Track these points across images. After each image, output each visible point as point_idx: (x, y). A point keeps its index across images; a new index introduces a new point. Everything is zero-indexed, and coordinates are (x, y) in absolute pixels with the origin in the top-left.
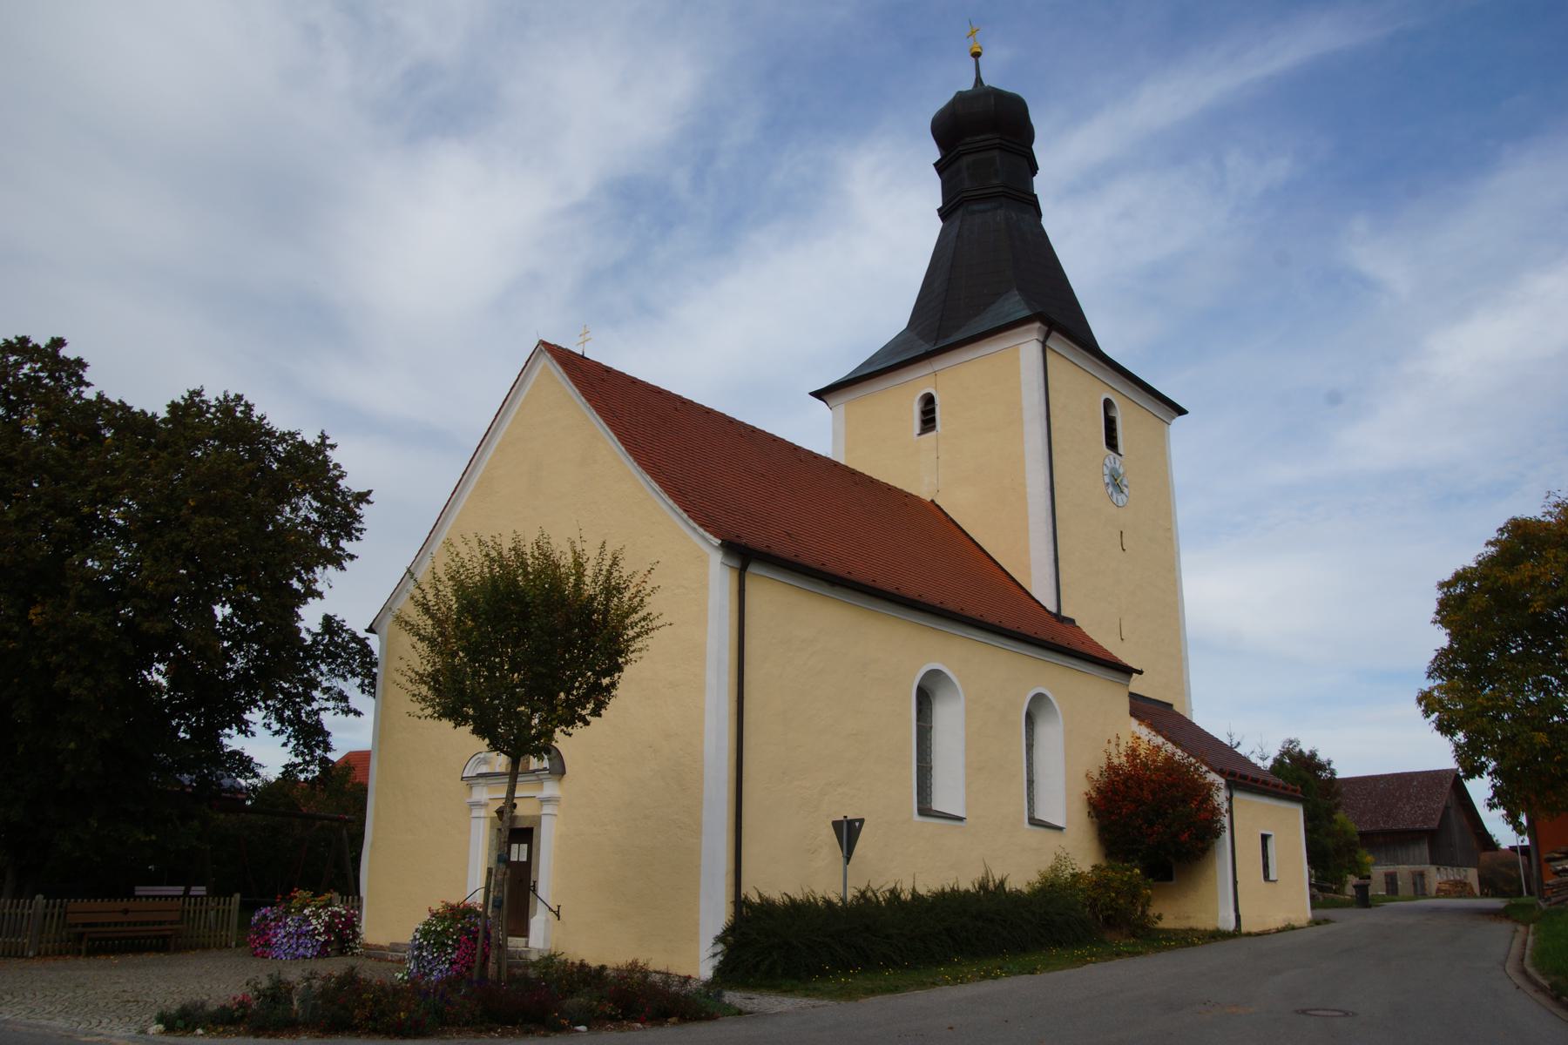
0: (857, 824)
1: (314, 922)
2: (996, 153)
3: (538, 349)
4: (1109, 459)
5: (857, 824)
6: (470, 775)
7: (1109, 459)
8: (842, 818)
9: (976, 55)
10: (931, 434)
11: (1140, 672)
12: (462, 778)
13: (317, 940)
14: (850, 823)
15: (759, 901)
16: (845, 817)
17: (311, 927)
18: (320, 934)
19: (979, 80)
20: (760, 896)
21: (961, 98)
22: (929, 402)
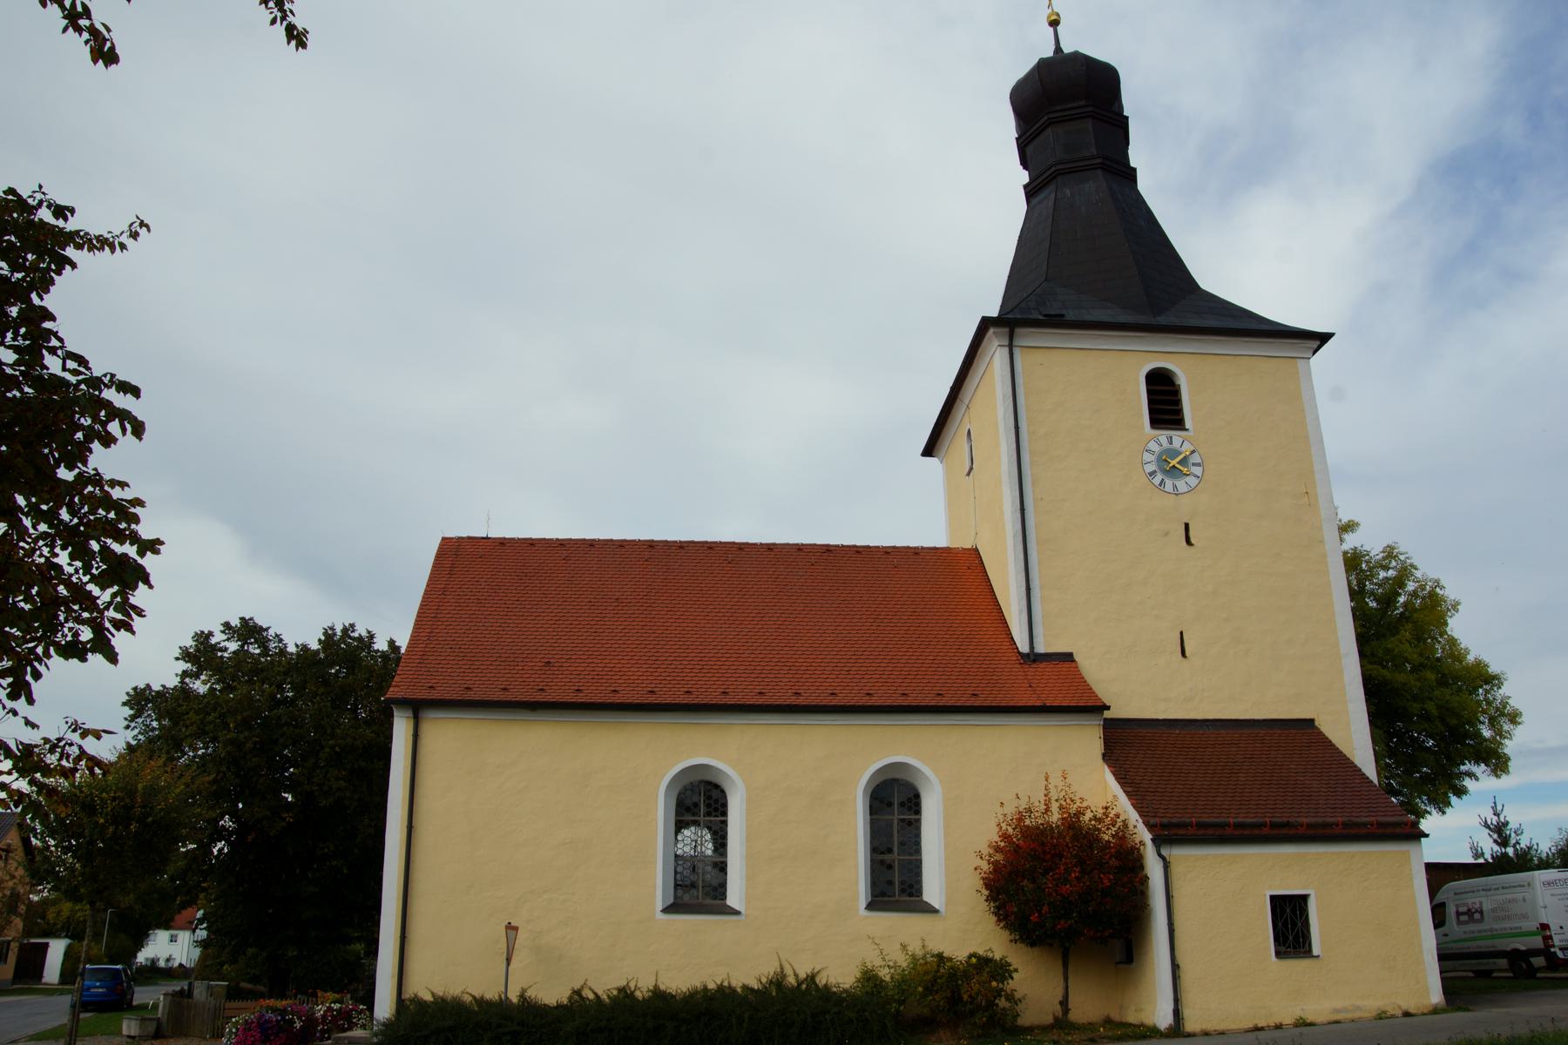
15: (432, 999)
19: (1058, 49)
20: (433, 994)
21: (1043, 65)
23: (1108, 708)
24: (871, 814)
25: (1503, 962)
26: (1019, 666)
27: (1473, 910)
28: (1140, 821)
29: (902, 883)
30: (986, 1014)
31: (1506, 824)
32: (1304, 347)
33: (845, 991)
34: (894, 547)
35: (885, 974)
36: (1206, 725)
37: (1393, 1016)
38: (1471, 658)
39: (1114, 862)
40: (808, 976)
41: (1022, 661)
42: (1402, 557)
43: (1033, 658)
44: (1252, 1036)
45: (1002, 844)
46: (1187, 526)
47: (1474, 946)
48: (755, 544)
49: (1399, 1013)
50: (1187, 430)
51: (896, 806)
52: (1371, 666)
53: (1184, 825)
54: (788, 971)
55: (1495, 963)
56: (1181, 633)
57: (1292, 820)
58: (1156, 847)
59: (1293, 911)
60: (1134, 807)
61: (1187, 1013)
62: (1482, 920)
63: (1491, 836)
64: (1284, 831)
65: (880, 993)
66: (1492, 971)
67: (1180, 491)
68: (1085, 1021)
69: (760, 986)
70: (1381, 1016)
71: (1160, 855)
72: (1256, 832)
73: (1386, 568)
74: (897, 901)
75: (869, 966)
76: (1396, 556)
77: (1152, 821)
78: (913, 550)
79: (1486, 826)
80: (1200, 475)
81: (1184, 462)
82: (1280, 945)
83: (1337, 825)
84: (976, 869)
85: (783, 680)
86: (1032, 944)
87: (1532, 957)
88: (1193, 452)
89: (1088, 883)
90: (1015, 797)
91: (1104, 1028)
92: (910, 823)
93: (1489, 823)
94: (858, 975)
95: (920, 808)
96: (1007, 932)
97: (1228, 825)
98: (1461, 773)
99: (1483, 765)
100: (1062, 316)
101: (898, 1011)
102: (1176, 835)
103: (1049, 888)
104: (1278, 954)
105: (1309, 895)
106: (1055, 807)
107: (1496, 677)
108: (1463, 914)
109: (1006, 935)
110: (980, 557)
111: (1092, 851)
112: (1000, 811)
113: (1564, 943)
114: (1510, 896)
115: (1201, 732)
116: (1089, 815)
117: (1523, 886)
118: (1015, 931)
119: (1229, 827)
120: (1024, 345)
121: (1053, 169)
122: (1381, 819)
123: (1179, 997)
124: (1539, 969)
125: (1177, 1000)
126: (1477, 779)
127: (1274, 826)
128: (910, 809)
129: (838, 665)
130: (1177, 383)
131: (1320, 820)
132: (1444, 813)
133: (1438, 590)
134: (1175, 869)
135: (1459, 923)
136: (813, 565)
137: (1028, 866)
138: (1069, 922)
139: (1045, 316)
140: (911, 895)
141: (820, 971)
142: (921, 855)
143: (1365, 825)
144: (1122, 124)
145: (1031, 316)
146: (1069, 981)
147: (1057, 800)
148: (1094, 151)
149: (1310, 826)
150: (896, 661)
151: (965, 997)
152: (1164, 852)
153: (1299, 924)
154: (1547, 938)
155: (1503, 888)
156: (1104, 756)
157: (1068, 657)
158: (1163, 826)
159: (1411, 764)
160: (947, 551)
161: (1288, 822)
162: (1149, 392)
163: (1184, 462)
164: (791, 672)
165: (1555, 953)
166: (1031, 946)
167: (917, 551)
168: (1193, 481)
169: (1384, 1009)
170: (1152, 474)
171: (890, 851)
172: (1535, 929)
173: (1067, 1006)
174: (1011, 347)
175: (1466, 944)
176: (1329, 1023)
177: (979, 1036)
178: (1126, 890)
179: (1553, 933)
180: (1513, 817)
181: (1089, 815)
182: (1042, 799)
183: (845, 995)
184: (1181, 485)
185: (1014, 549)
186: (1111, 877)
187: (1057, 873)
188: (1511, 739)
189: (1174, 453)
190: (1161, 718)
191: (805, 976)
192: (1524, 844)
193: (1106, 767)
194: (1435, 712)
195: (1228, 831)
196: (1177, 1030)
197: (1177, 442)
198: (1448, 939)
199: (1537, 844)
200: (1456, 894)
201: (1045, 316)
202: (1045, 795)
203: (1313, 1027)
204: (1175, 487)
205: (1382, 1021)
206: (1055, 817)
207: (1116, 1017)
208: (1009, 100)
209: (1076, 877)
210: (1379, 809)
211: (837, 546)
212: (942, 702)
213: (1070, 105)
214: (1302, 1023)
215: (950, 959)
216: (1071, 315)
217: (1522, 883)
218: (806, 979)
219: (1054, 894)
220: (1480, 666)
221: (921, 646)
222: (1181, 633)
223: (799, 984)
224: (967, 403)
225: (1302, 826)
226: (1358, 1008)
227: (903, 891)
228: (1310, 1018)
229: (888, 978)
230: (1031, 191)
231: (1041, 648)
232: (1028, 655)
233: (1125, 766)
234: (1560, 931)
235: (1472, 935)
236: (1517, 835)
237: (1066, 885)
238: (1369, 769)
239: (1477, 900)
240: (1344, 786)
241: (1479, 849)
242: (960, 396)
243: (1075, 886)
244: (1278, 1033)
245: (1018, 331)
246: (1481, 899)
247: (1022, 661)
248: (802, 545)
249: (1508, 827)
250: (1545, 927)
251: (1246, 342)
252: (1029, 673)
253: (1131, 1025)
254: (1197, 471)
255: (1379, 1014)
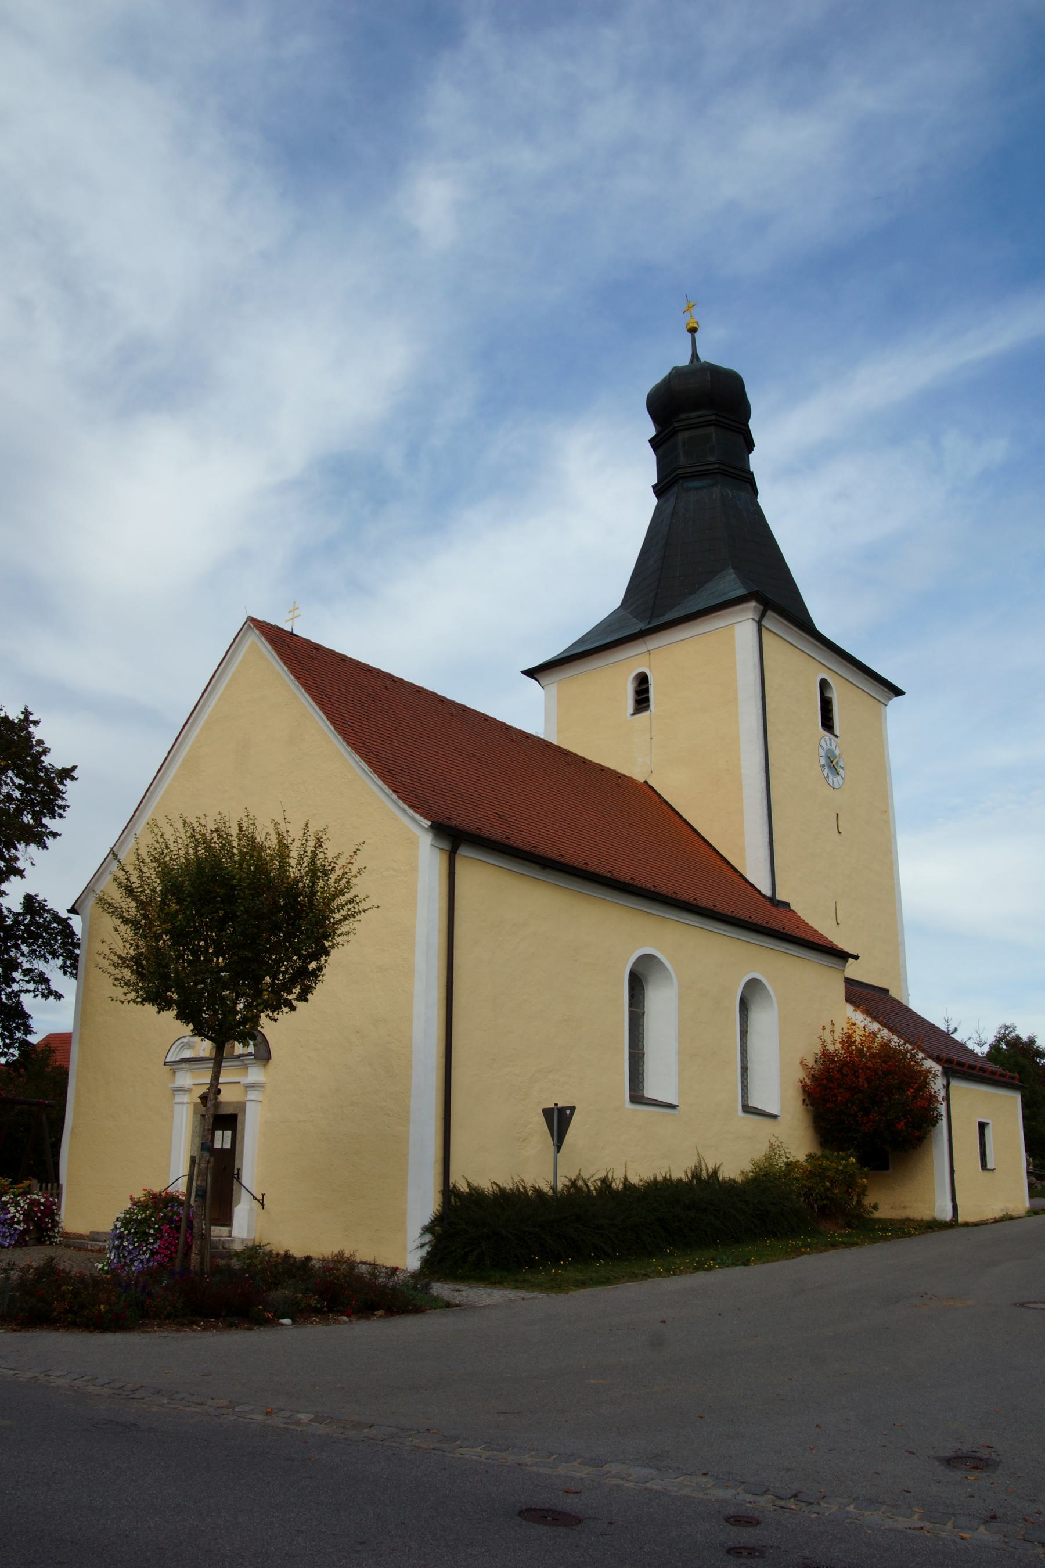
0: (568, 1112)
1: (12, 1210)
2: (712, 430)
3: (246, 626)
4: (825, 740)
5: (568, 1112)
6: (173, 1060)
7: (825, 740)
8: (553, 1106)
9: (693, 331)
10: (645, 715)
11: (856, 957)
12: (165, 1063)
13: (16, 1229)
14: (561, 1111)
16: (556, 1105)
17: (9, 1216)
18: (18, 1223)
19: (695, 356)
20: (469, 1184)
21: (677, 374)
22: (642, 682)
68: (919, 1218)
69: (687, 1179)
141: (720, 1165)
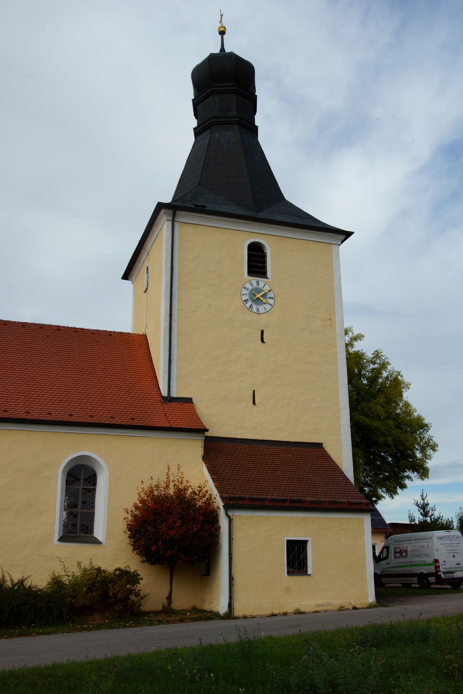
23: (207, 430)
24: (66, 485)
25: (415, 579)
26: (161, 404)
27: (403, 551)
28: (218, 495)
29: (82, 525)
30: (122, 604)
31: (427, 505)
32: (337, 239)
33: (40, 590)
34: (98, 330)
35: (66, 580)
36: (263, 443)
37: (347, 609)
38: (416, 414)
39: (201, 518)
40: (19, 581)
41: (163, 401)
42: (383, 358)
43: (169, 399)
44: (269, 619)
45: (141, 505)
46: (262, 332)
47: (401, 570)
48: (15, 322)
49: (350, 607)
50: (268, 278)
51: (82, 480)
52: (360, 417)
53: (242, 499)
54: (7, 578)
55: (411, 580)
56: (254, 391)
57: (301, 499)
58: (225, 510)
59: (299, 549)
60: (216, 487)
61: (236, 605)
62: (406, 556)
63: (419, 511)
64: (297, 505)
65: (61, 591)
66: (411, 584)
67: (260, 312)
68: (181, 609)
70: (341, 609)
71: (227, 515)
72: (282, 504)
73: (374, 363)
74: (78, 536)
75: (57, 574)
76: (380, 357)
77: (224, 495)
78: (108, 333)
79: (417, 505)
80: (272, 304)
81: (264, 296)
82: (290, 568)
83: (326, 503)
84: (125, 519)
85: (20, 404)
86: (153, 563)
87: (429, 577)
88: (270, 291)
89: (185, 530)
90: (151, 478)
91: (190, 613)
92: (89, 491)
93: (419, 503)
94: (50, 580)
95: (96, 482)
96: (139, 556)
97: (266, 500)
98: (404, 477)
99: (416, 473)
100: (205, 207)
101: (71, 603)
102: (237, 504)
103: (163, 531)
104: (289, 573)
105: (308, 540)
106: (172, 484)
107: (426, 425)
108: (398, 552)
109: (138, 558)
110: (147, 340)
111: (189, 511)
112: (141, 486)
113: (445, 570)
114: (421, 544)
115: (260, 447)
116: (190, 490)
117: (428, 539)
118: (143, 556)
119: (267, 501)
120: (180, 221)
121: (210, 121)
122: (350, 500)
123: (232, 596)
124: (433, 584)
125: (231, 598)
126: (412, 480)
127: (291, 501)
128: (90, 482)
129: (55, 397)
130: (265, 251)
131: (317, 499)
132: (393, 498)
133: (399, 377)
134: (236, 524)
135: (395, 557)
136: (48, 337)
137: (152, 518)
138: (173, 551)
139: (195, 205)
140: (86, 533)
141: (29, 577)
142: (94, 510)
143: (341, 503)
144: (253, 100)
145: (187, 205)
146: (173, 585)
147: (173, 481)
148: (235, 113)
149: (311, 502)
150: (90, 397)
151: (111, 594)
152: (230, 513)
153: (302, 556)
154: (437, 567)
155: (418, 539)
156: (203, 457)
157: (189, 400)
158: (230, 499)
159: (377, 470)
160: (128, 334)
161: (300, 499)
162: (249, 255)
163: (264, 296)
164: (25, 399)
165: (440, 575)
166: (152, 565)
167: (111, 334)
168: (268, 307)
169: (343, 605)
170: (246, 301)
171: (76, 506)
172: (432, 562)
173: (171, 600)
174: (173, 221)
175: (399, 569)
176: (313, 612)
177: (117, 618)
178: (207, 534)
179: (440, 564)
180: (431, 500)
181: (190, 490)
182: (165, 480)
183: (40, 593)
184: (262, 309)
185: (164, 338)
186: (199, 526)
187: (168, 523)
188: (430, 459)
189: (259, 290)
190: (238, 437)
191: (17, 581)
192: (436, 515)
193: (204, 464)
194: (391, 443)
195: (266, 503)
196: (229, 615)
197: (261, 284)
198: (389, 566)
199: (442, 516)
200: (395, 541)
201: (195, 205)
202: (167, 478)
203: (318, 613)
204: (258, 309)
205: (341, 611)
206: (171, 491)
207: (199, 606)
208: (190, 76)
209: (179, 526)
210: (350, 494)
211: (64, 327)
212: (113, 422)
213: (224, 84)
214: (298, 612)
215: (104, 572)
216: (209, 207)
217: (427, 538)
218: (18, 583)
219: (166, 535)
220: (419, 419)
221: (106, 389)
222: (254, 391)
223: (14, 586)
224: (148, 251)
225: (307, 502)
226: (330, 604)
227: (82, 530)
228: (303, 610)
229: (67, 583)
230: (198, 132)
231: (174, 394)
232: (166, 398)
233: (215, 464)
234: (444, 563)
235: (401, 564)
236: (433, 511)
237: (173, 530)
238: (349, 473)
239: (405, 545)
240: (324, 481)
241: (413, 517)
242: (144, 247)
243: (178, 531)
244: (284, 618)
245: (178, 213)
246: (407, 545)
247: (163, 401)
248: (43, 325)
249: (429, 507)
250: (436, 561)
251: (305, 232)
252: (166, 408)
253: (206, 611)
254: (271, 301)
255: (340, 608)
